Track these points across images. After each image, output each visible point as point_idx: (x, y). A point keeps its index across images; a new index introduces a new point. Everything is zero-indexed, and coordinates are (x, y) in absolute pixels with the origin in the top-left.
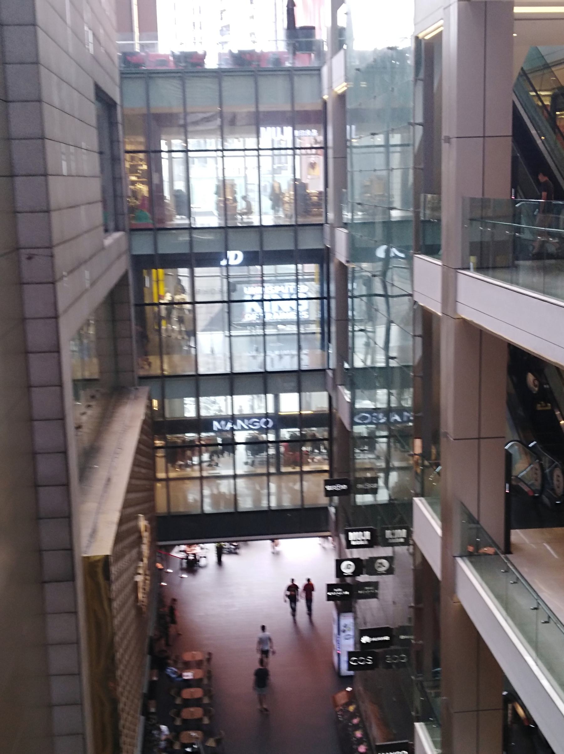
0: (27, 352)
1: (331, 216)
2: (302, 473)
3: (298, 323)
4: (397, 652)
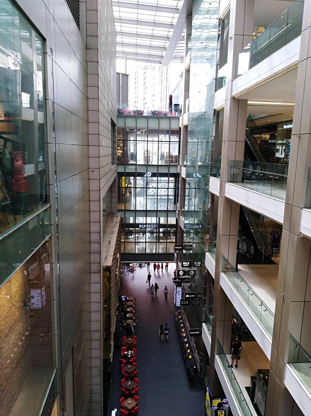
0: (90, 201)
1: (180, 163)
2: (167, 242)
3: (168, 195)
4: (196, 301)
